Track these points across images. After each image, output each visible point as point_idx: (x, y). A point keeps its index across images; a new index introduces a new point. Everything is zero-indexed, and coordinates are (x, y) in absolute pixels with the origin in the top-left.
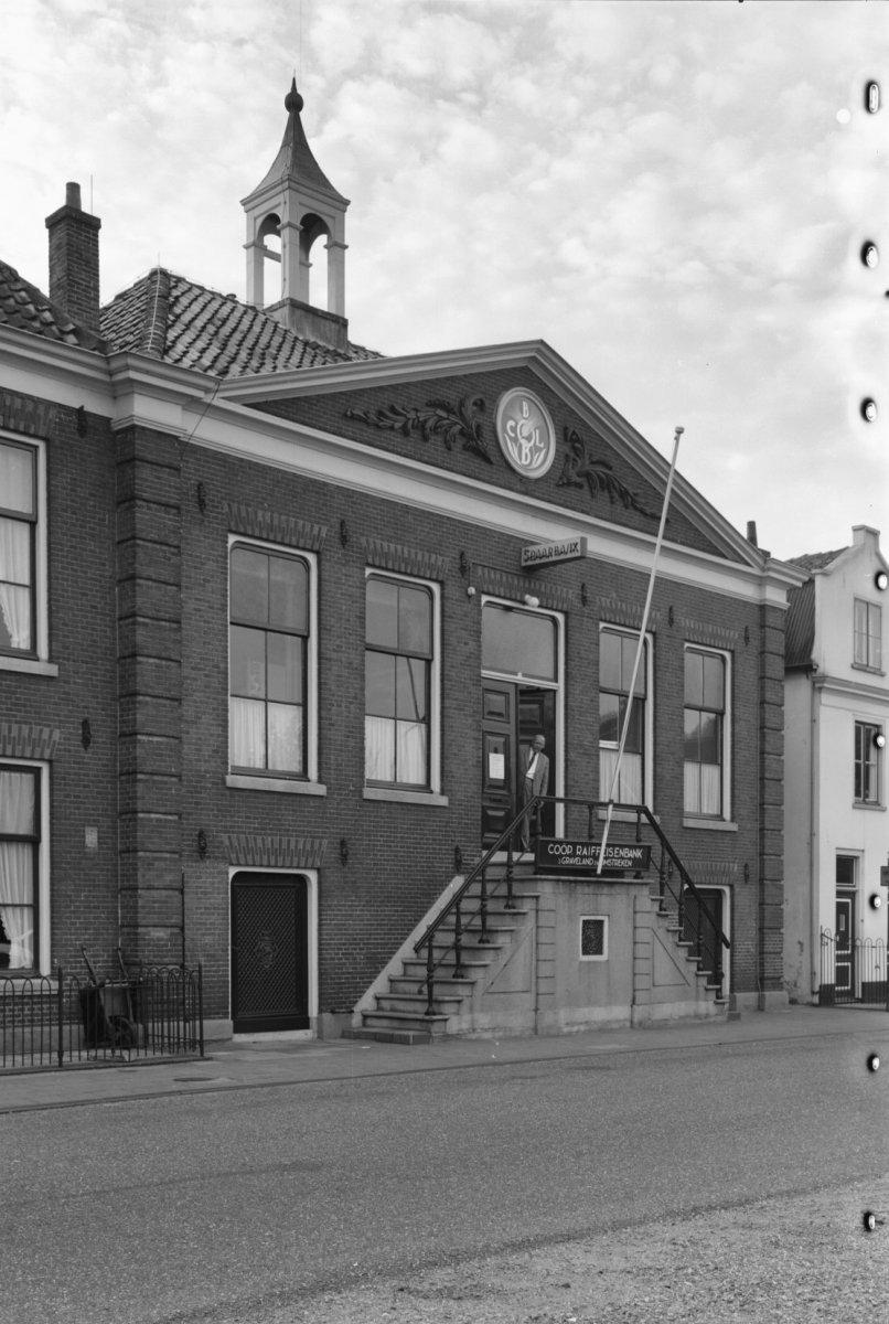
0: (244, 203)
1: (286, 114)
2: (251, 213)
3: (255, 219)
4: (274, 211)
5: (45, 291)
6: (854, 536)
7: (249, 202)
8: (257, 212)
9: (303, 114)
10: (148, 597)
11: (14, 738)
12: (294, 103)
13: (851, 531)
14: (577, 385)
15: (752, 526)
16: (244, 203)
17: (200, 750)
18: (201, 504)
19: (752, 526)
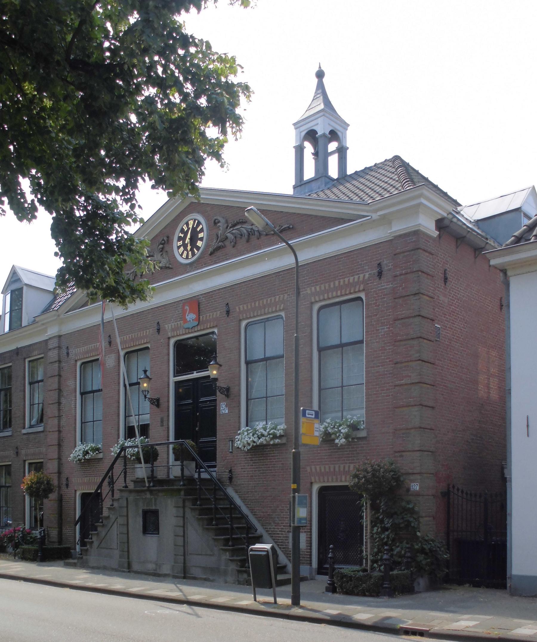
0: (294, 124)
1: (316, 80)
2: (298, 130)
3: (301, 132)
4: (314, 128)
5: (114, 192)
6: (296, 131)
7: (297, 124)
8: (302, 129)
9: (325, 80)
10: (180, 541)
11: (346, 471)
12: (320, 75)
13: (293, 127)
14: (299, 123)
15: (184, 22)
16: (294, 124)
17: (489, 379)
18: (446, 279)
19: (184, 22)
